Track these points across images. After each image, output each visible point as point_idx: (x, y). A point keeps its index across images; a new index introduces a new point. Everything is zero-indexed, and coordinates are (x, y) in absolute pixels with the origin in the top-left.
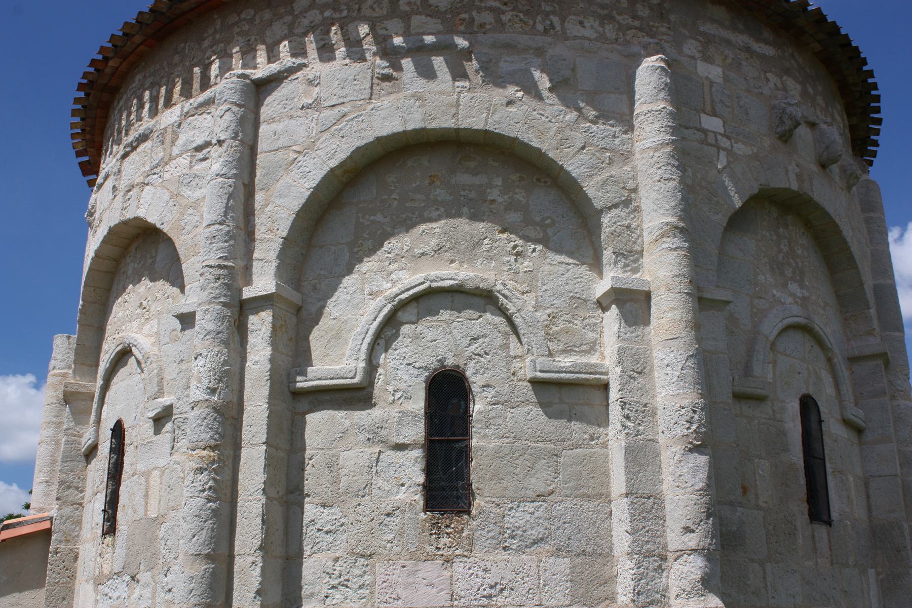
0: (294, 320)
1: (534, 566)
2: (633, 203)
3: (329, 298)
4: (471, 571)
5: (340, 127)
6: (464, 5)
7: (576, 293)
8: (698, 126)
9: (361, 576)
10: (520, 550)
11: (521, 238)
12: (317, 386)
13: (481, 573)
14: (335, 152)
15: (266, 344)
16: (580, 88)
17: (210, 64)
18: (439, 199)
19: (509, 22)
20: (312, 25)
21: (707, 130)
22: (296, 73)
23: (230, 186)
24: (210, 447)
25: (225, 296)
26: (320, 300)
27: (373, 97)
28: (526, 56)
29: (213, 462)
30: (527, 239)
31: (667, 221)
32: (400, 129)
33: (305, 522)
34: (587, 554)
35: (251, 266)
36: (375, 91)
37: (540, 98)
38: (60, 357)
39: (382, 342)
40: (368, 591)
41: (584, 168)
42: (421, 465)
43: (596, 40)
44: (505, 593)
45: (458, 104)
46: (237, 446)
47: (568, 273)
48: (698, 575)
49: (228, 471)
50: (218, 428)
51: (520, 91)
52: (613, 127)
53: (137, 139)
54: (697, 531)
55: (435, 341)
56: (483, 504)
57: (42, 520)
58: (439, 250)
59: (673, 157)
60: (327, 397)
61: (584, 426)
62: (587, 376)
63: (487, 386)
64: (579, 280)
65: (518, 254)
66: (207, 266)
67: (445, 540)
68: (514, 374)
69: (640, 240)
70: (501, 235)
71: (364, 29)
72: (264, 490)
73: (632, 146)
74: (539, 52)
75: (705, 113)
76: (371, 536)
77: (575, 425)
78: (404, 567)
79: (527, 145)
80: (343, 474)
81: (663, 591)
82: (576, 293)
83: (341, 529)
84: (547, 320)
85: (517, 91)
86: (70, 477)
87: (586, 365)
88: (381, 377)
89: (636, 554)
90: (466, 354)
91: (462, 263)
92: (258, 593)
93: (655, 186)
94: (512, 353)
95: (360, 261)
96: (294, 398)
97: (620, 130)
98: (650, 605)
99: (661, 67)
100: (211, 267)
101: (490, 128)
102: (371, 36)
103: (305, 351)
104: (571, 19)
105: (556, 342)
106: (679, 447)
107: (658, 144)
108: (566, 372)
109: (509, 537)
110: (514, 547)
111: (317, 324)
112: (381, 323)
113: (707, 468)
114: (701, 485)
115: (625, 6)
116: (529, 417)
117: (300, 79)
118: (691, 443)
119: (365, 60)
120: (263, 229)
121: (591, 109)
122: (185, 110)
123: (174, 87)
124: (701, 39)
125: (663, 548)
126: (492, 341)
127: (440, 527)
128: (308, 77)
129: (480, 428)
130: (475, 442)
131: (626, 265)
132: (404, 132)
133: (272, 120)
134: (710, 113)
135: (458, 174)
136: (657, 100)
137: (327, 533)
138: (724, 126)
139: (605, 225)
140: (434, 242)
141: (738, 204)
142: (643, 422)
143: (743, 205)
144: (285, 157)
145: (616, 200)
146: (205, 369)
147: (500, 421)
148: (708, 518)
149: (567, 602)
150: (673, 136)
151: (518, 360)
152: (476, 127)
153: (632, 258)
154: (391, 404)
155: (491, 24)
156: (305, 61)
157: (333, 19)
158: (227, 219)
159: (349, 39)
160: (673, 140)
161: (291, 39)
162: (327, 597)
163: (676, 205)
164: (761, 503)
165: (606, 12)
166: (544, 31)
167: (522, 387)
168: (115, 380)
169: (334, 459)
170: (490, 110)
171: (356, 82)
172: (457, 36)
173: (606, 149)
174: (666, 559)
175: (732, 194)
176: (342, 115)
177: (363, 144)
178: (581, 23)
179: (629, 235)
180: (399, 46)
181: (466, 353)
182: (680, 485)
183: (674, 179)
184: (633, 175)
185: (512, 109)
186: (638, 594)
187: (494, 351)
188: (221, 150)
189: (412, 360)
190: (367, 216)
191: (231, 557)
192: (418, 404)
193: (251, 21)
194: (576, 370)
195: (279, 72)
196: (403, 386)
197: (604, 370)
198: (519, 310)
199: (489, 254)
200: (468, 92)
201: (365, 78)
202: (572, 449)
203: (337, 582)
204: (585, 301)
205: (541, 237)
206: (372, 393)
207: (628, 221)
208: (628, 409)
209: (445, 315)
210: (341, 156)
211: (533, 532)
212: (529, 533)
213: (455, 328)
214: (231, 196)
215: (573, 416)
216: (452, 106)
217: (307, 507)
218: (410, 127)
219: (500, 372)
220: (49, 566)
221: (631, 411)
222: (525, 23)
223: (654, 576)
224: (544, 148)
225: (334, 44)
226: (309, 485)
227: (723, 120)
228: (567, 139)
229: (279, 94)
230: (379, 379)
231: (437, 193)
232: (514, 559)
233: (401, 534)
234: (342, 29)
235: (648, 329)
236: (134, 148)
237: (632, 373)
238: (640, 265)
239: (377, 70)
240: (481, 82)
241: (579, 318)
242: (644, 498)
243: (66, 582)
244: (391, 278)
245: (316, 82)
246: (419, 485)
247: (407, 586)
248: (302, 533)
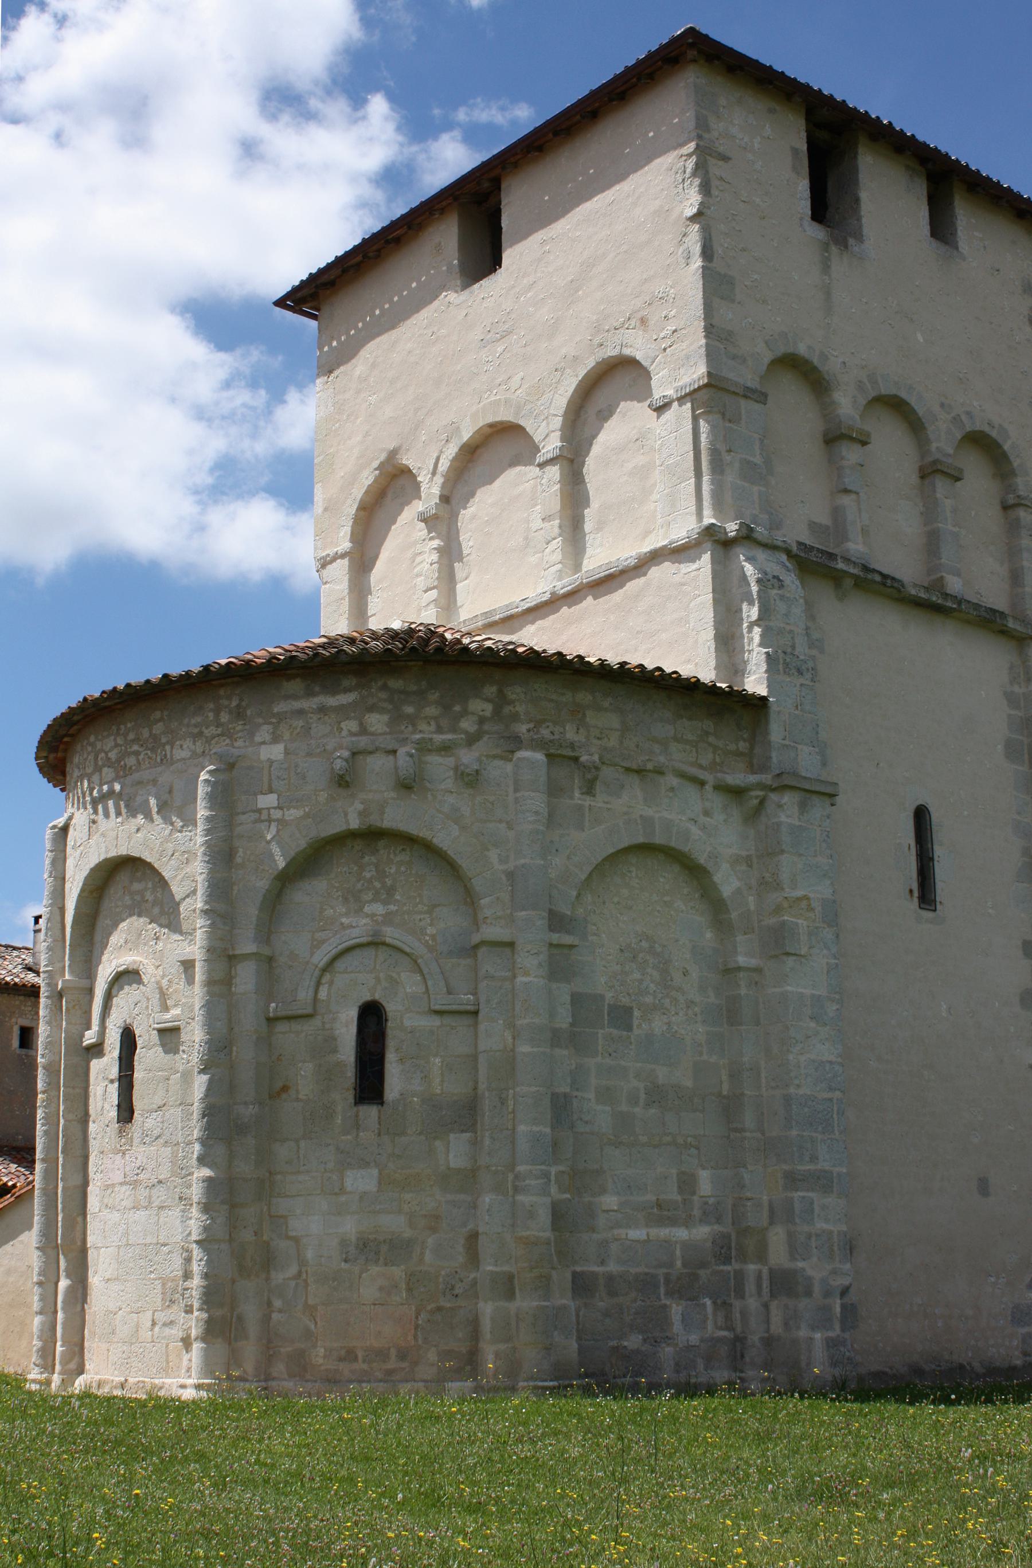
10: (150, 1144)
59: (205, 854)
74: (155, 782)
138: (278, 800)
141: (281, 863)
148: (203, 1118)
164: (300, 1096)
175: (277, 858)
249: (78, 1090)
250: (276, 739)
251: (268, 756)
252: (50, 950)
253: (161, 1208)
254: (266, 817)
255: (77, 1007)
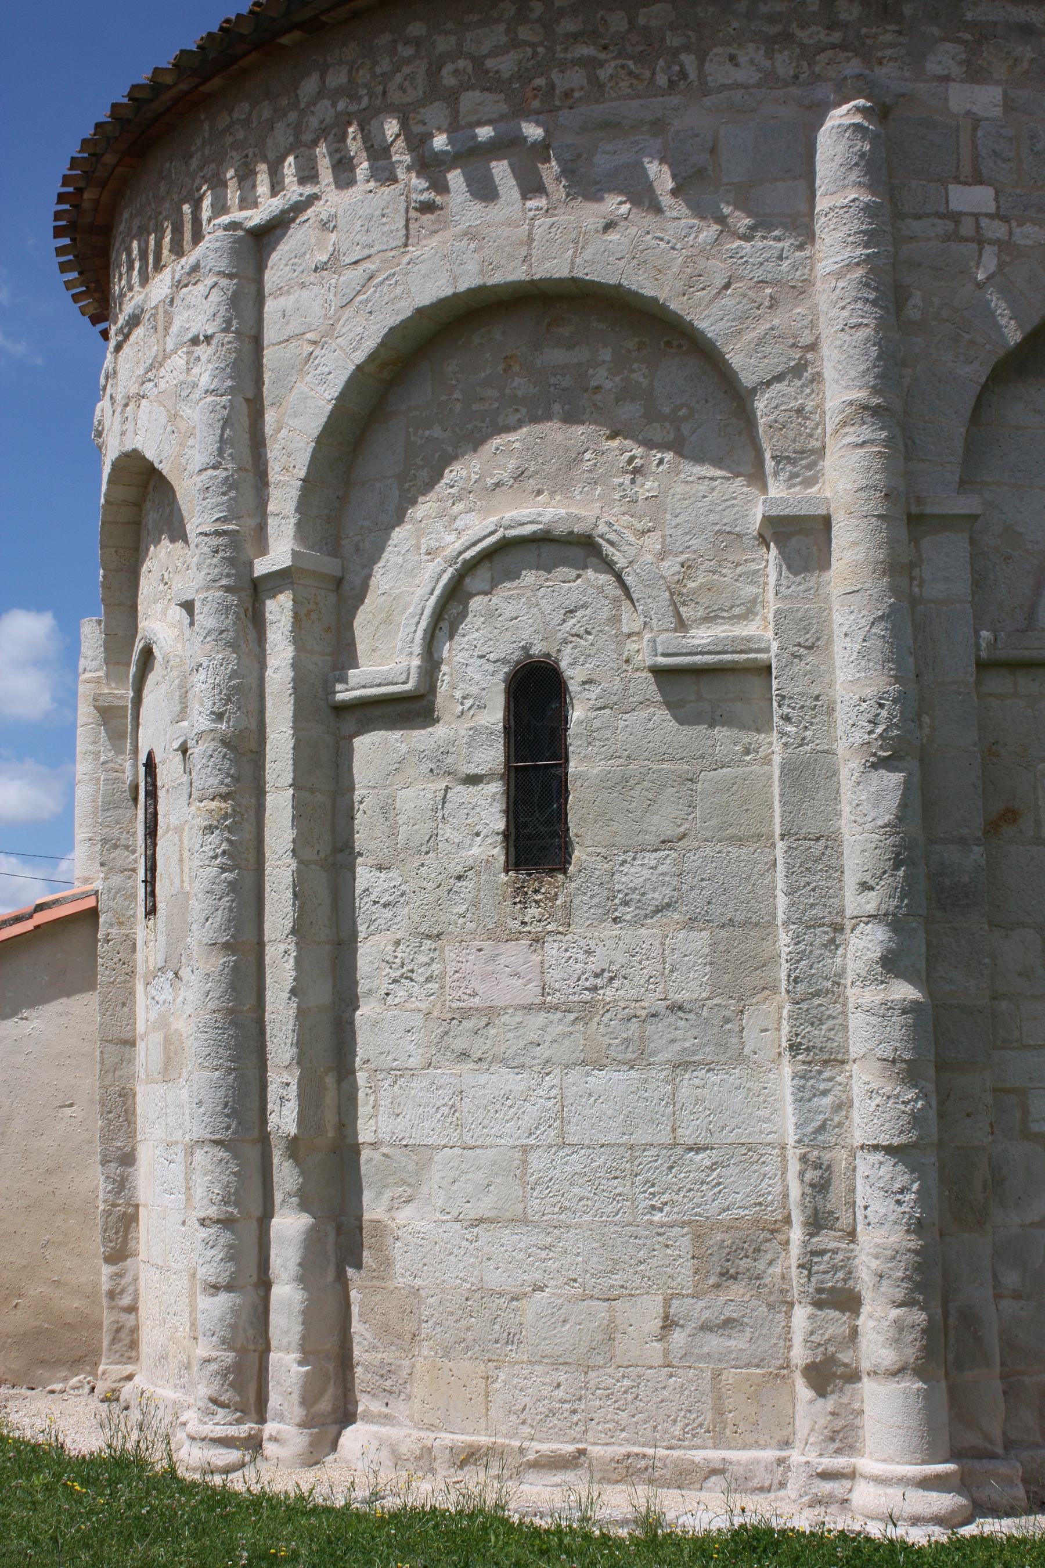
0: (332, 598)
1: (657, 943)
2: (809, 369)
3: (376, 563)
4: (568, 954)
5: (365, 297)
6: (538, 62)
7: (725, 525)
8: (942, 209)
9: (428, 964)
10: (638, 922)
11: (641, 443)
12: (361, 698)
13: (581, 957)
14: (362, 338)
15: (286, 642)
16: (725, 180)
17: (201, 199)
18: (519, 393)
19: (609, 81)
20: (323, 126)
21: (960, 214)
22: (305, 211)
23: (224, 407)
24: (220, 796)
25: (228, 576)
26: (364, 566)
27: (410, 241)
28: (637, 138)
29: (226, 817)
30: (649, 444)
31: (851, 398)
32: (448, 292)
33: (358, 892)
34: (736, 924)
35: (266, 524)
36: (412, 232)
37: (657, 209)
38: (90, 653)
39: (445, 625)
40: (437, 985)
41: (728, 321)
42: (500, 805)
43: (759, 85)
44: (616, 983)
45: (530, 239)
46: (260, 792)
47: (714, 494)
48: (876, 952)
49: (249, 828)
50: (230, 769)
51: (625, 202)
52: (779, 240)
53: (128, 323)
54: (878, 887)
55: (516, 618)
56: (584, 857)
57: (86, 895)
58: (519, 476)
59: (867, 285)
60: (377, 712)
61: (735, 732)
62: (736, 657)
63: (590, 682)
64: (729, 503)
65: (636, 471)
66: (201, 533)
67: (533, 911)
68: (627, 661)
69: (819, 431)
70: (610, 443)
71: (391, 127)
72: (293, 851)
73: (811, 270)
74: (658, 127)
75: (959, 183)
76: (438, 908)
77: (720, 733)
78: (480, 950)
79: (636, 294)
80: (401, 822)
81: (835, 976)
82: (725, 525)
83: (402, 900)
84: (679, 573)
85: (621, 203)
86: (115, 832)
87: (734, 639)
88: (445, 677)
89: (794, 923)
90: (560, 635)
91: (552, 494)
92: (293, 992)
93: (836, 339)
94: (625, 630)
95: (414, 502)
96: (338, 716)
97: (792, 244)
98: (814, 996)
99: (854, 124)
100: (206, 535)
101: (579, 274)
102: (402, 137)
103: (349, 645)
104: (715, 55)
105: (693, 605)
106: (858, 761)
107: (843, 267)
108: (702, 653)
109: (621, 904)
110: (628, 917)
111: (362, 602)
112: (440, 598)
113: (900, 792)
114: (887, 818)
115: (815, 8)
116: (650, 725)
117: (311, 221)
118: (874, 755)
119: (395, 180)
120: (277, 469)
121: (743, 215)
122: (177, 278)
123: (163, 238)
124: (967, 36)
125: (837, 913)
126: (595, 612)
127: (526, 893)
128: (321, 217)
129: (580, 746)
130: (574, 767)
131: (794, 476)
132: (455, 295)
133: (280, 292)
134: (970, 180)
135: (546, 350)
136: (845, 187)
137: (385, 906)
138: (996, 199)
139: (759, 414)
140: (512, 464)
141: (1014, 335)
142: (812, 724)
143: (1024, 339)
144: (298, 351)
145: (780, 369)
146: (208, 685)
147: (608, 734)
148: (896, 867)
149: (704, 995)
150: (869, 248)
151: (634, 638)
152: (557, 276)
153: (804, 462)
154: (459, 717)
155: (582, 88)
156: (315, 190)
157: (349, 114)
158: (223, 458)
159: (372, 146)
160: (868, 255)
161: (298, 152)
162: (387, 994)
163: (868, 369)
165: (778, 28)
166: (669, 86)
167: (640, 680)
168: (145, 692)
169: (390, 801)
170: (577, 243)
171: (384, 220)
172: (527, 121)
173: (766, 282)
174: (843, 929)
175: (1003, 322)
176: (368, 276)
177: (397, 322)
178: (732, 58)
179: (800, 424)
180: (442, 151)
181: (560, 634)
182: (858, 819)
183: (866, 325)
184: (811, 322)
185: (613, 236)
186: (796, 981)
187: (599, 628)
188: (210, 350)
189: (485, 650)
190: (420, 432)
191: (260, 946)
192: (494, 716)
193: (247, 123)
194: (718, 649)
195: (283, 212)
196: (474, 690)
197: (762, 646)
198: (631, 562)
199: (591, 476)
200: (546, 217)
201: (397, 211)
202: (715, 770)
203: (398, 973)
204: (739, 536)
205: (671, 439)
206: (433, 703)
207: (800, 402)
208: (789, 706)
209: (529, 577)
210: (370, 344)
211: (656, 895)
212: (649, 897)
213: (543, 597)
214: (226, 423)
215: (717, 718)
216: (522, 244)
217: (359, 870)
218: (462, 287)
219: (608, 659)
220: (100, 960)
221: (794, 708)
222: (637, 77)
223: (821, 955)
224: (662, 296)
225: (353, 158)
226: (361, 840)
227: (995, 188)
228: (700, 276)
229: (287, 248)
230: (443, 681)
231: (515, 384)
232: (628, 935)
233: (475, 904)
234: (362, 130)
235: (826, 576)
236: (127, 337)
237: (796, 648)
238: (818, 472)
239: (414, 196)
240: (564, 196)
241: (729, 565)
242: (810, 839)
243: (125, 982)
244: (455, 526)
245: (332, 225)
246: (498, 834)
247: (485, 977)
248: (354, 908)
249: (319, 797)
250: (975, 74)
251: (968, 106)
252: (231, 488)
253: (682, 1065)
254: (972, 233)
255: (314, 616)
